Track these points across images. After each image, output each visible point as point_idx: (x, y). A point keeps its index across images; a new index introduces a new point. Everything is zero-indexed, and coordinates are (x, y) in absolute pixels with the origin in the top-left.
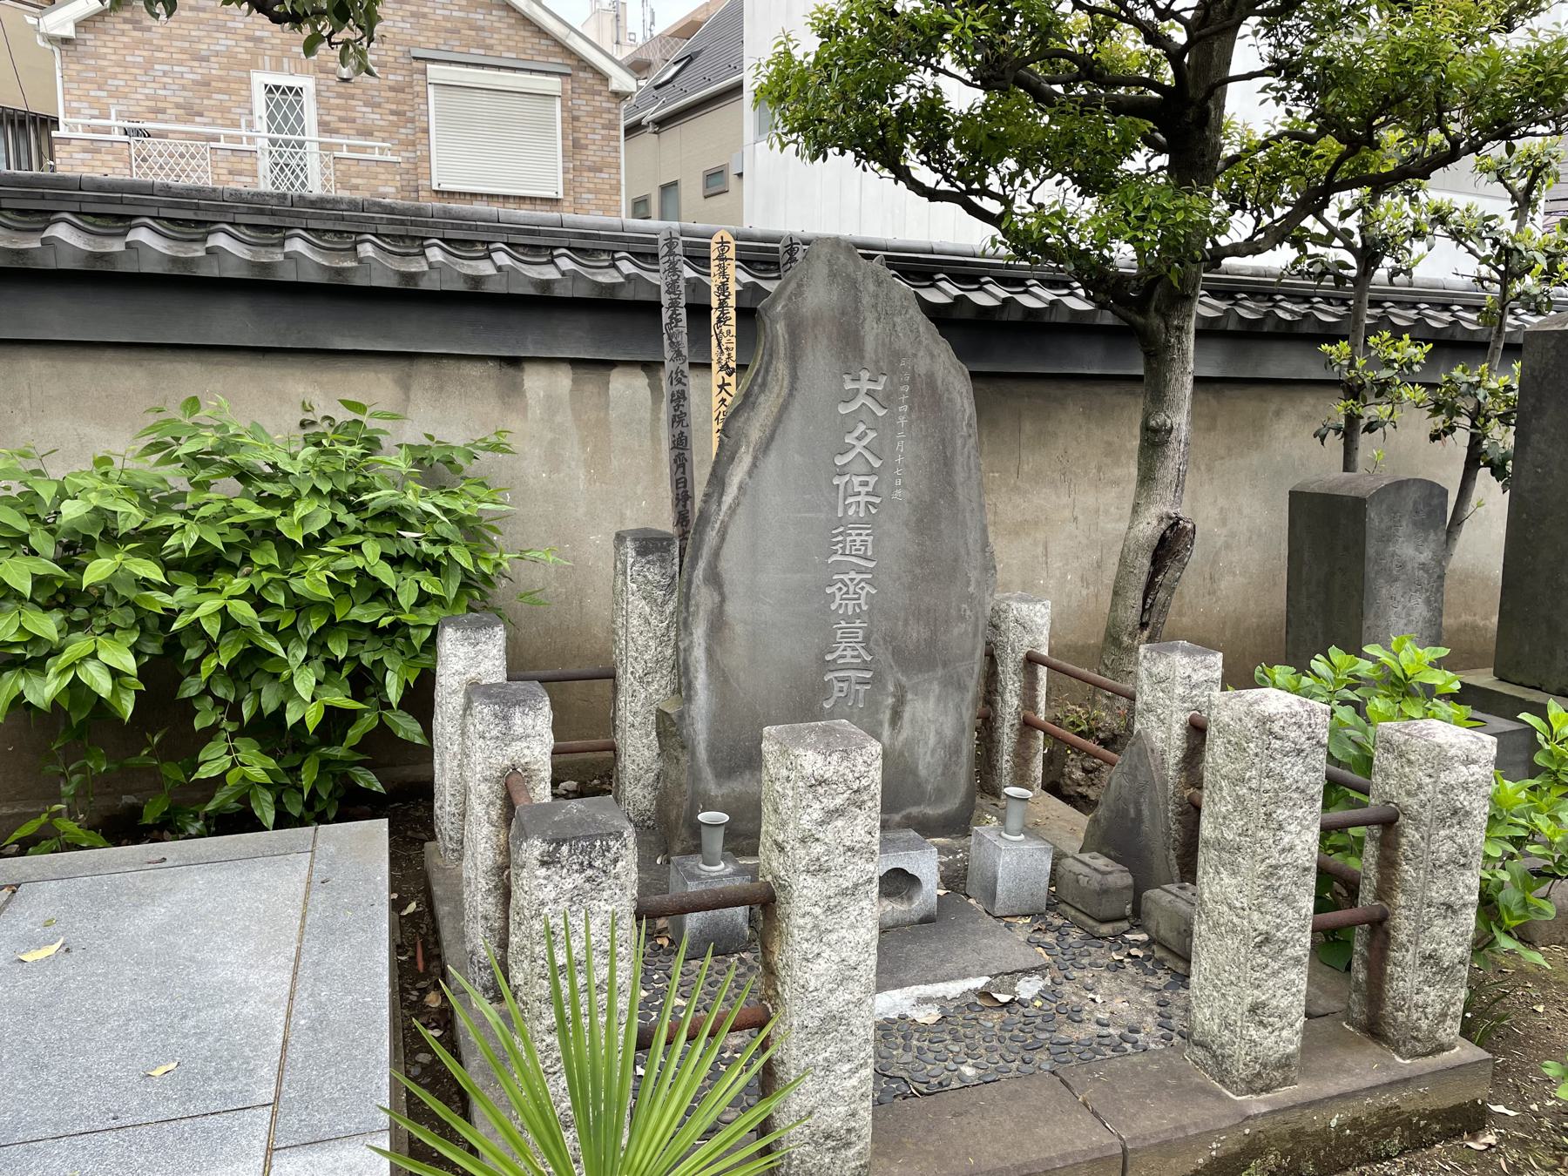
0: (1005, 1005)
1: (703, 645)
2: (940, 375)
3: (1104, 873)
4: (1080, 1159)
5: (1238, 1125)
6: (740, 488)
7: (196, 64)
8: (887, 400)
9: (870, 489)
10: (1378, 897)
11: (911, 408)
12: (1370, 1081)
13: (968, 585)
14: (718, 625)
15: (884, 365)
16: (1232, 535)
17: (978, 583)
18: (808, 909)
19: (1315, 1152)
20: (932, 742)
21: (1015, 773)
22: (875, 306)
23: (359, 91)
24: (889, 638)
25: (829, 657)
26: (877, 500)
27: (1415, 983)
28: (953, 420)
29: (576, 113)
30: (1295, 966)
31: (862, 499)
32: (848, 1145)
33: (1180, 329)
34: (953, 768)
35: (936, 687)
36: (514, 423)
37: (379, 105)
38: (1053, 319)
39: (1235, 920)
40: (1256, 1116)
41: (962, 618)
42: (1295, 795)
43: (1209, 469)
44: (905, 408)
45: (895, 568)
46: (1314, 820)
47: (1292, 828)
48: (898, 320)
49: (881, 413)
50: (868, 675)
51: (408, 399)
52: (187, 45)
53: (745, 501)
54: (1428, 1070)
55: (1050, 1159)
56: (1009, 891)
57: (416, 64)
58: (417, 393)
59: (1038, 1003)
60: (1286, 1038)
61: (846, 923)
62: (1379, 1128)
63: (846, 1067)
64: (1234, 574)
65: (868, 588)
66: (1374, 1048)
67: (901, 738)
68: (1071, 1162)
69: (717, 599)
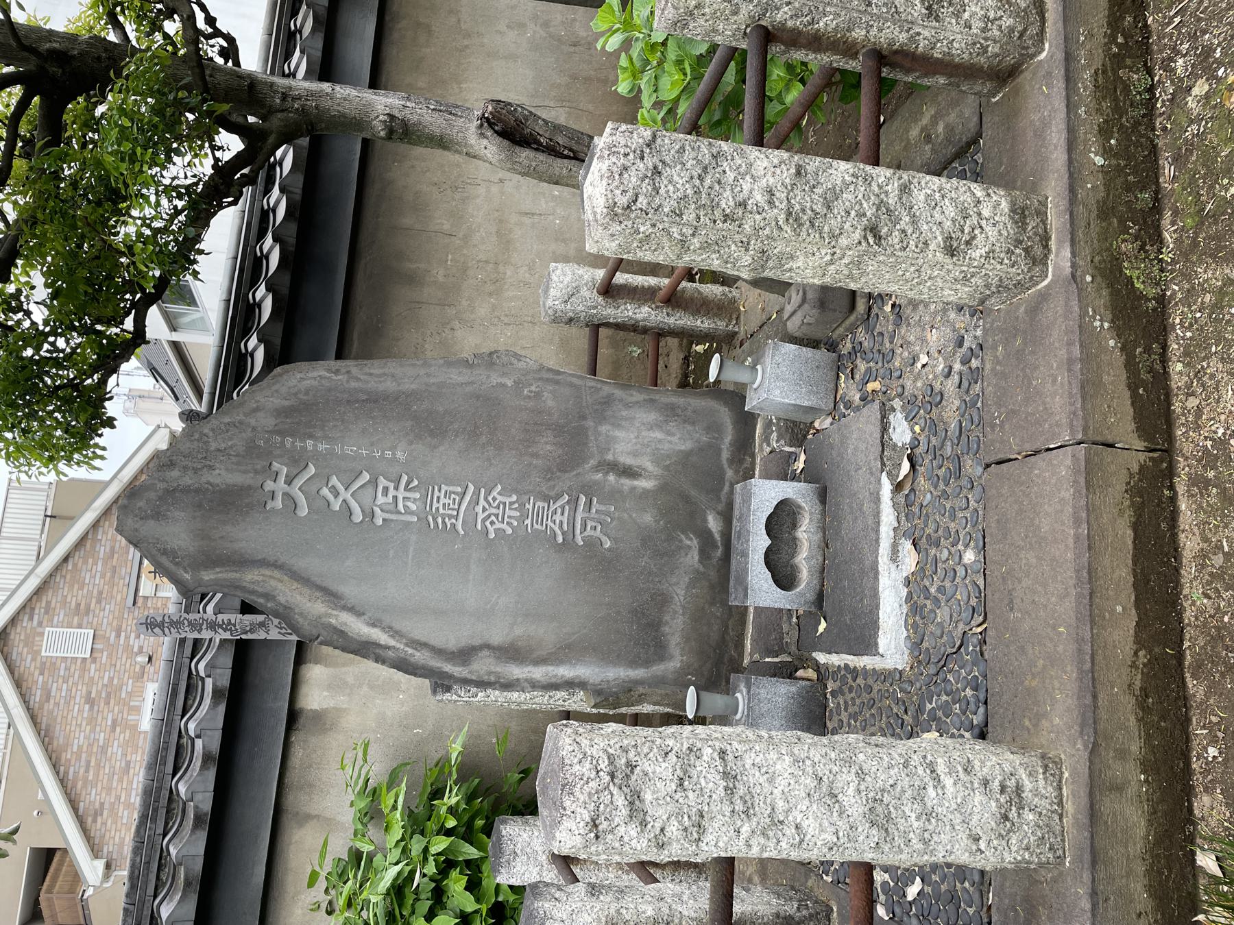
0: (913, 466)
1: (530, 668)
2: (277, 402)
3: (804, 300)
4: (1083, 502)
5: (1080, 290)
6: (373, 625)
7: (131, 771)
8: (298, 462)
9: (392, 485)
10: (854, 56)
11: (311, 437)
12: (1060, 105)
13: (503, 385)
14: (512, 653)
15: (260, 464)
16: (535, 17)
17: (504, 374)
18: (742, 843)
19: (1128, 188)
20: (658, 435)
21: (716, 315)
22: (196, 471)
24: (549, 474)
25: (560, 539)
26: (405, 478)
27: (957, 29)
28: (329, 390)
30: (910, 194)
31: (401, 494)
32: (1019, 789)
33: (284, 96)
34: (689, 413)
35: (604, 429)
36: (351, 722)
38: (299, 191)
39: (846, 261)
40: (1074, 265)
41: (538, 395)
42: (708, 182)
43: (468, 35)
44: (310, 442)
45: (478, 462)
46: (742, 155)
47: (746, 187)
48: (213, 446)
49: (312, 470)
50: (583, 499)
51: (317, 817)
52: (116, 777)
53: (387, 620)
54: (1060, 25)
55: (1077, 538)
56: (810, 392)
57: (140, 602)
58: (313, 809)
59: (917, 428)
60: (992, 207)
61: (767, 788)
62: (1116, 100)
63: (931, 792)
64: (574, 20)
65: (494, 493)
66: (1025, 77)
67: (649, 466)
68: (1084, 515)
69: (485, 652)
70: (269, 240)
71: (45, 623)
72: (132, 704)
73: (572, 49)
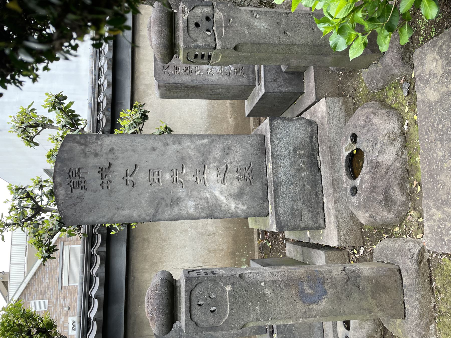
23: (72, 304)
43: (165, 240)
57: (63, 288)
64: (207, 224)
70: (101, 115)
71: (30, 299)
72: (65, 325)
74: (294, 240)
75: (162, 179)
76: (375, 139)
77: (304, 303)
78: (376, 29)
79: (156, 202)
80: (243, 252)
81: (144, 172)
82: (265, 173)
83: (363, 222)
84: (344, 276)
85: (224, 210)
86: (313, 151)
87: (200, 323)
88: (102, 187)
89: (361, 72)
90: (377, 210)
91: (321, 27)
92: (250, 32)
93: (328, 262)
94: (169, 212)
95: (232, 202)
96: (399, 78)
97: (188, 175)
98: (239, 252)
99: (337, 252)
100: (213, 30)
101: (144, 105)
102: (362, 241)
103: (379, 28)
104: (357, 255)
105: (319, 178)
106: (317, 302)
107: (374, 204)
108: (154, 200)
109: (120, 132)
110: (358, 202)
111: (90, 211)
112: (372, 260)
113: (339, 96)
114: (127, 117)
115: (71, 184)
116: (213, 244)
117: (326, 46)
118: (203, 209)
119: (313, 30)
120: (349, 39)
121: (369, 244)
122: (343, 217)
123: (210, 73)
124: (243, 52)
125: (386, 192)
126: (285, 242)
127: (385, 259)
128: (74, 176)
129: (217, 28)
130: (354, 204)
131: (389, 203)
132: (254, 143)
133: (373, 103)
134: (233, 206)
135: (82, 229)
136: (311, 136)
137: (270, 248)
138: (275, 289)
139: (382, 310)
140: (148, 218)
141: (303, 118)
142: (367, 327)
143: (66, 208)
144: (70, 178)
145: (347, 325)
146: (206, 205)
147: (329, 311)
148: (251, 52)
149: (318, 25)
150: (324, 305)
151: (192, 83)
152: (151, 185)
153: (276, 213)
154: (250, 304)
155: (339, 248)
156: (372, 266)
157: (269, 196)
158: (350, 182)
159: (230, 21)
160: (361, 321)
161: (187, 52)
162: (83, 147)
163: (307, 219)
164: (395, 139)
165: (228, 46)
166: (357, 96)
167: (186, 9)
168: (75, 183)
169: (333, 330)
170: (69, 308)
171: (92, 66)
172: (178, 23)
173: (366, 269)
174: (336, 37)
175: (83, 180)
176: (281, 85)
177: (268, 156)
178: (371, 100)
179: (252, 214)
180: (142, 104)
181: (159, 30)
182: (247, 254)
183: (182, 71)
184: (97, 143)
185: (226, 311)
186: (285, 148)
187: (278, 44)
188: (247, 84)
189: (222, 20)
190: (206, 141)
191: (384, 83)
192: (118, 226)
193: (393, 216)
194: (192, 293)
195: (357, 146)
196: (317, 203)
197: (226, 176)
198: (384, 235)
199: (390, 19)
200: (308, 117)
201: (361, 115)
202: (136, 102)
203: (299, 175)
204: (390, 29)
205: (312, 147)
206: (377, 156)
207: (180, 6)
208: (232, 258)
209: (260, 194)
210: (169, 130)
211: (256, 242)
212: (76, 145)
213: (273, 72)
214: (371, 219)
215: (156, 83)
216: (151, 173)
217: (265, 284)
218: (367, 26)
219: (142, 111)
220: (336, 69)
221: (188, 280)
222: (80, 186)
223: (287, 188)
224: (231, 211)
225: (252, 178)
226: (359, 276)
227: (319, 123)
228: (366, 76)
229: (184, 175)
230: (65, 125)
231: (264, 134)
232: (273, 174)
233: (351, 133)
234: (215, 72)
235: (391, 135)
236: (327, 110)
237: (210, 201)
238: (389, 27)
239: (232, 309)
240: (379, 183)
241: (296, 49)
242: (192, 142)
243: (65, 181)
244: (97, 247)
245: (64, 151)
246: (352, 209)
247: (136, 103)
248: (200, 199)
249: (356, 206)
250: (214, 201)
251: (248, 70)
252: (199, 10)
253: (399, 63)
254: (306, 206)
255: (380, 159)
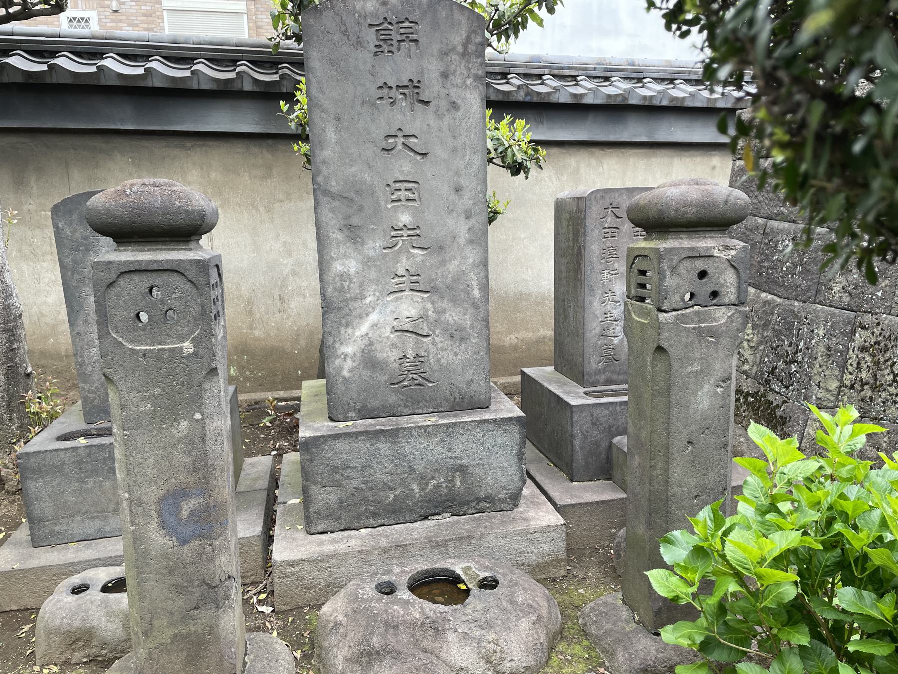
23: (124, 18)
29: (260, 24)
37: (137, 26)
43: (269, 210)
64: (305, 296)
73: (277, 297)
74: (280, 473)
75: (398, 206)
76: (489, 625)
77: (161, 500)
78: (241, 535)
79: (353, 195)
80: (249, 369)
81: (412, 171)
82: (416, 411)
83: (325, 608)
84: (217, 578)
85: (339, 332)
86: (462, 504)
87: (113, 292)
88: (381, 88)
89: (615, 591)
90: (350, 635)
91: (705, 514)
92: (691, 375)
93: (244, 544)
94: (333, 222)
95: (356, 348)
96: (607, 664)
97: (408, 259)
98: (248, 361)
99: (261, 560)
100: (693, 306)
101: (540, 167)
102: (285, 608)
103: (705, 624)
104: (255, 599)
105: (408, 518)
106: (163, 525)
107: (362, 629)
108: (357, 192)
109: (488, 120)
110: (365, 597)
111: (333, 63)
112: (250, 629)
113: (568, 550)
114: (517, 133)
115: (386, 25)
116: (263, 309)
117: (667, 522)
118: (341, 290)
119: (696, 497)
120: (685, 569)
121: (280, 623)
122: (332, 569)
123: (608, 299)
124: (652, 364)
125: (387, 651)
126: (274, 453)
127: (252, 656)
128: (402, 31)
129: (698, 313)
130: (361, 589)
131: (366, 659)
132: (474, 387)
133: (557, 617)
134: (349, 349)
135: (289, 42)
136: (489, 499)
137: (269, 426)
138: (188, 440)
139: (150, 656)
140: (320, 179)
141: (525, 483)
142: (110, 626)
143: (338, 15)
144: (398, 23)
145: (117, 586)
146: (348, 296)
147: (145, 551)
148: (652, 380)
149: (709, 507)
150: (158, 539)
151: (587, 263)
152: (388, 185)
153: (336, 437)
154: (157, 391)
155: (267, 563)
156: (238, 632)
157: (370, 421)
158: (405, 579)
159: (711, 337)
160: (121, 615)
161: (652, 256)
162: (460, 49)
163: (326, 497)
164: (491, 662)
165: (665, 335)
166: (569, 585)
167: (733, 252)
168: (387, 32)
169: (99, 559)
170: (116, 11)
171: (613, 63)
172: (705, 237)
173: (232, 620)
174: (688, 543)
175: (394, 49)
176: (585, 437)
177: (448, 416)
178: (562, 612)
179: (332, 388)
180: (542, 163)
181: (691, 202)
182: (246, 379)
183: (609, 244)
184: (469, 77)
185: (140, 343)
186: (464, 448)
187: (667, 430)
188: (587, 370)
189: (712, 322)
190: (476, 293)
191: (596, 636)
192: (297, 117)
193: (340, 668)
194: (176, 274)
195: (475, 590)
196: (358, 517)
197: (408, 334)
198: (299, 651)
199: (724, 644)
200: (525, 492)
201: (534, 594)
202: (545, 152)
203: (413, 479)
204: (707, 645)
205: (468, 503)
206: (456, 630)
207: (737, 242)
208: (236, 348)
209: (373, 404)
210: (493, 216)
211: (270, 396)
212: (464, 36)
213: (610, 421)
214: (332, 624)
215: (585, 192)
216: (410, 185)
217: (197, 421)
218: (712, 601)
219: (528, 163)
220: (619, 543)
221: (203, 266)
222: (381, 43)
223: (387, 456)
224: (337, 345)
225: (406, 386)
226: (218, 607)
227: (513, 514)
228: (610, 600)
229: (408, 252)
230: (497, 10)
231: (492, 407)
232: (414, 428)
233: (500, 577)
234: (609, 307)
235: (499, 655)
236: (542, 528)
237: (357, 304)
238: (710, 643)
239: (144, 355)
240: (403, 637)
241: (660, 465)
242: (475, 265)
243: (392, 12)
244: (251, 72)
245: (452, 10)
246: (351, 586)
247: (543, 152)
248: (361, 285)
249: (356, 594)
250: (359, 311)
251: (613, 372)
252: (730, 277)
253: (636, 663)
254: (353, 494)
255: (450, 636)
